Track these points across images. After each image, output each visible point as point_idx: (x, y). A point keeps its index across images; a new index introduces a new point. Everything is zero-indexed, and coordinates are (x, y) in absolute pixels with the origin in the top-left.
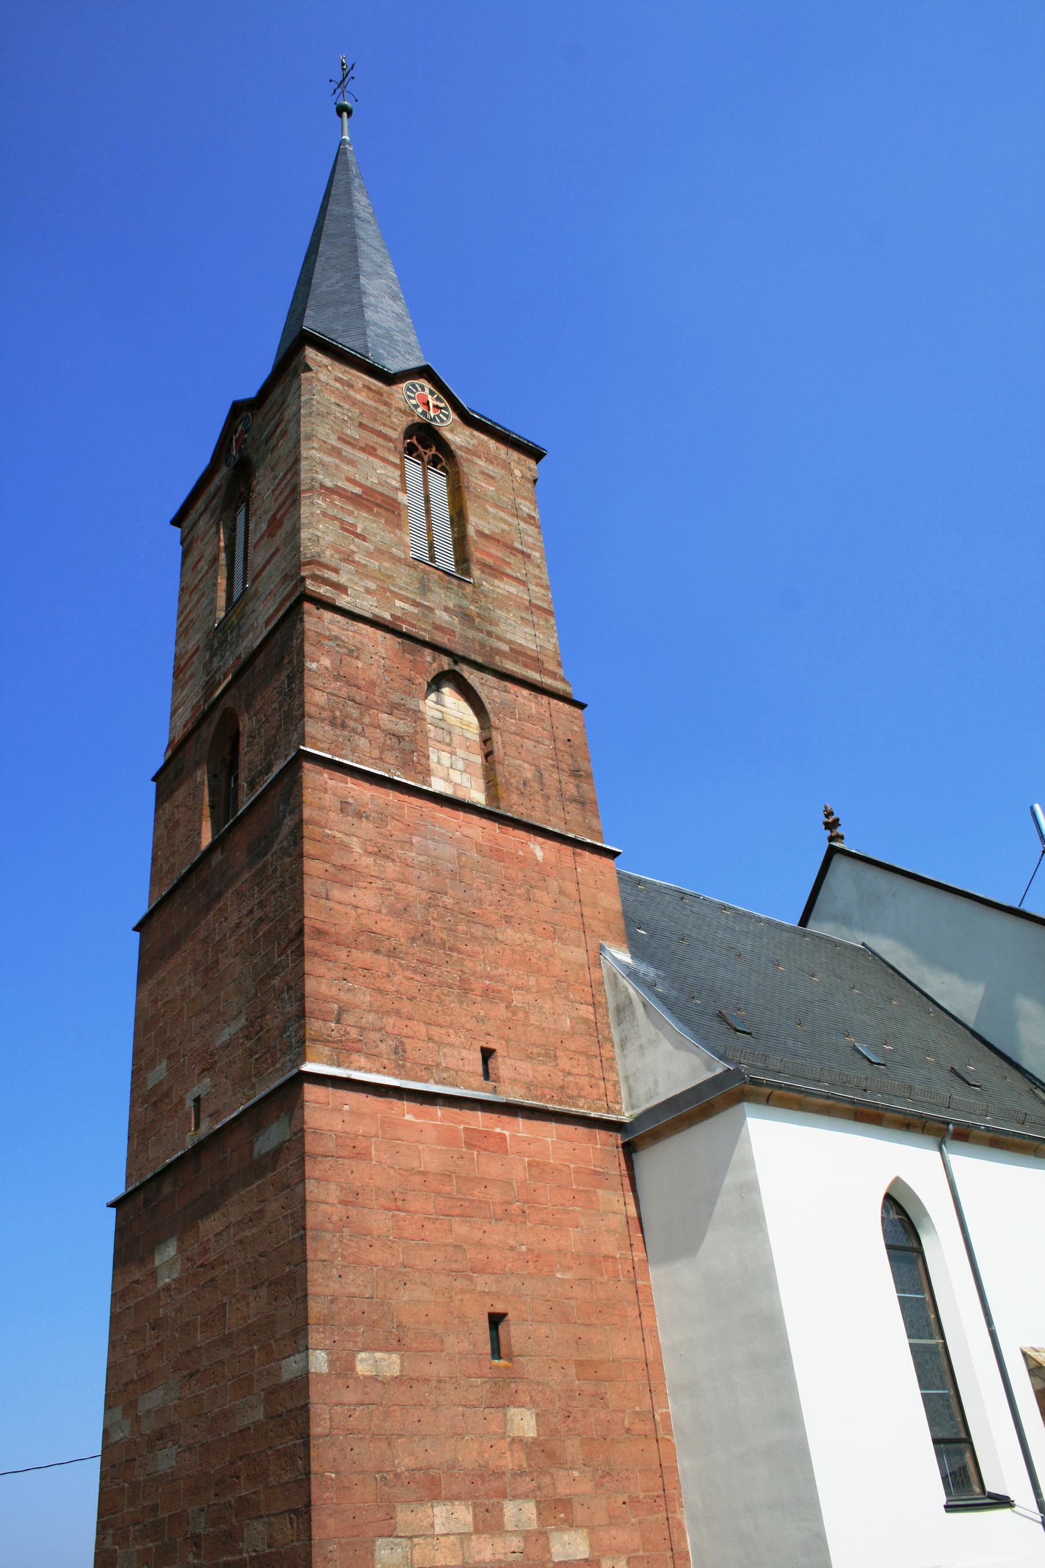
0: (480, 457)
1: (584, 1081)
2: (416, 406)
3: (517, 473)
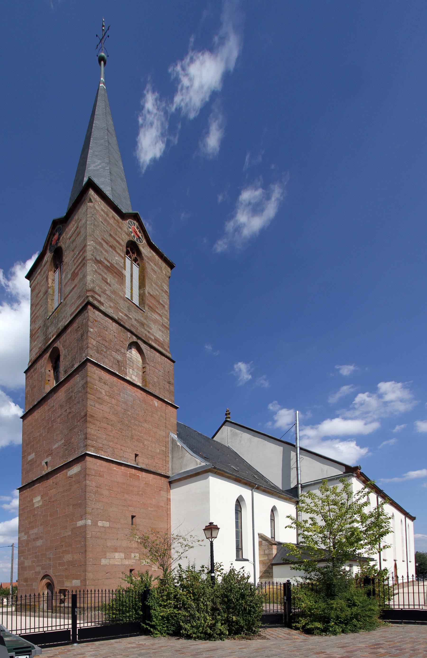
0: (152, 262)
1: (161, 465)
2: (132, 232)
3: (164, 272)
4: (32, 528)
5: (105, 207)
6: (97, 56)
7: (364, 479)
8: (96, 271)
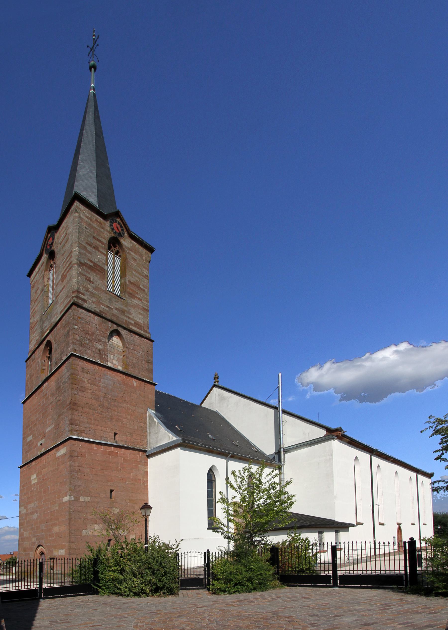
3: (144, 258)
4: (30, 503)
5: (89, 213)
6: (89, 63)
7: (348, 440)
8: (80, 273)
